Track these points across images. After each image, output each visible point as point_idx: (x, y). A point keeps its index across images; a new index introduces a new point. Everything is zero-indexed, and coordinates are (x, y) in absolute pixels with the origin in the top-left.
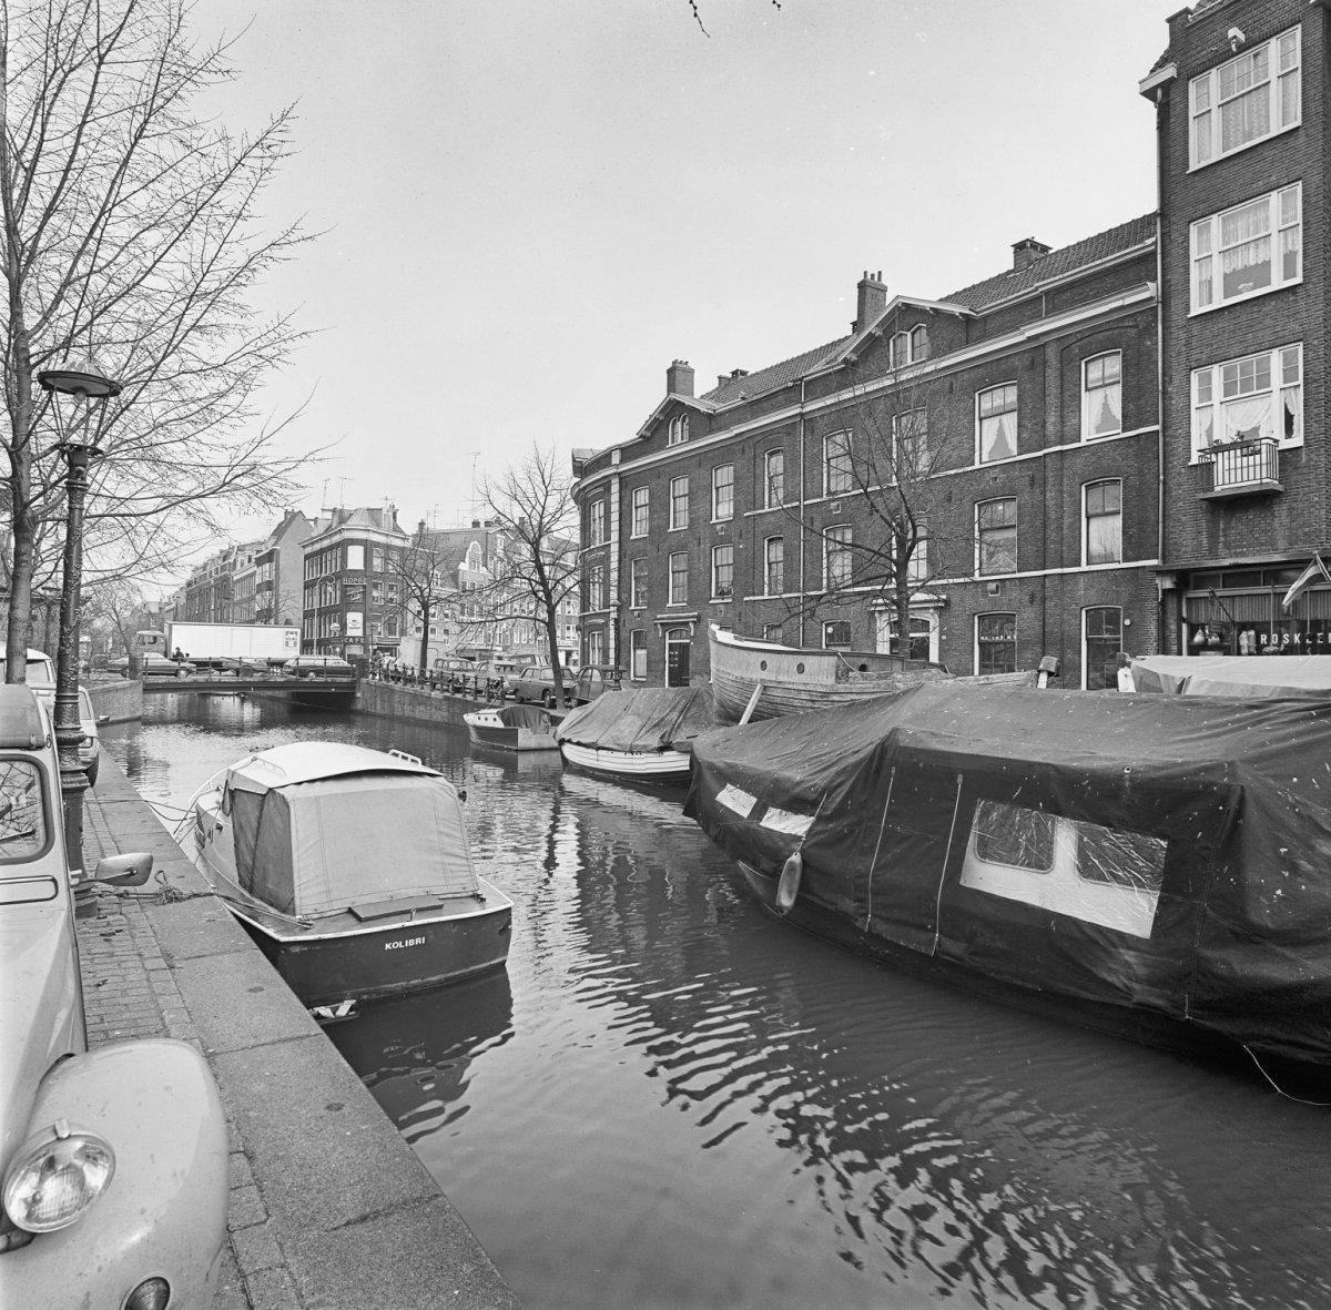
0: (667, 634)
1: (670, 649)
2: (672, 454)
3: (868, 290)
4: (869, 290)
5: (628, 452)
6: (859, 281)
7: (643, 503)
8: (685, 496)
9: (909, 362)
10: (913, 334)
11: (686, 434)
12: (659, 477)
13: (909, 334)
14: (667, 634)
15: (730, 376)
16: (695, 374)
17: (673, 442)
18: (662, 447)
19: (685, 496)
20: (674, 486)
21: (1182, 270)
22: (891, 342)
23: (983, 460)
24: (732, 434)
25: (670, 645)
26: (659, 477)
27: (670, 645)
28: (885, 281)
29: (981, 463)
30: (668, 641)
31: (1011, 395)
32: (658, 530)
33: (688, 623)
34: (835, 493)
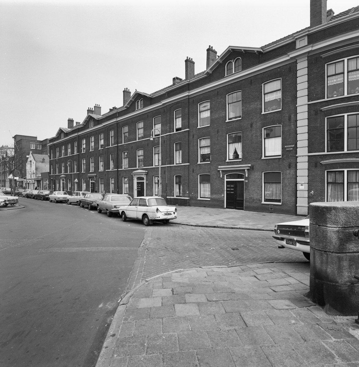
0: (90, 180)
1: (91, 184)
2: (63, 140)
3: (126, 93)
4: (189, 63)
5: (52, 140)
6: (207, 49)
7: (141, 127)
8: (142, 128)
9: (140, 108)
10: (141, 101)
11: (142, 106)
12: (87, 137)
13: (140, 101)
14: (90, 180)
15: (112, 109)
16: (101, 108)
17: (137, 109)
18: (134, 111)
19: (142, 128)
20: (91, 139)
21: (179, 92)
22: (136, 103)
23: (201, 125)
24: (102, 126)
25: (227, 181)
26: (87, 137)
27: (91, 182)
28: (130, 91)
29: (200, 126)
30: (90, 182)
31: (208, 105)
32: (96, 148)
33: (94, 177)
34: (231, 119)
